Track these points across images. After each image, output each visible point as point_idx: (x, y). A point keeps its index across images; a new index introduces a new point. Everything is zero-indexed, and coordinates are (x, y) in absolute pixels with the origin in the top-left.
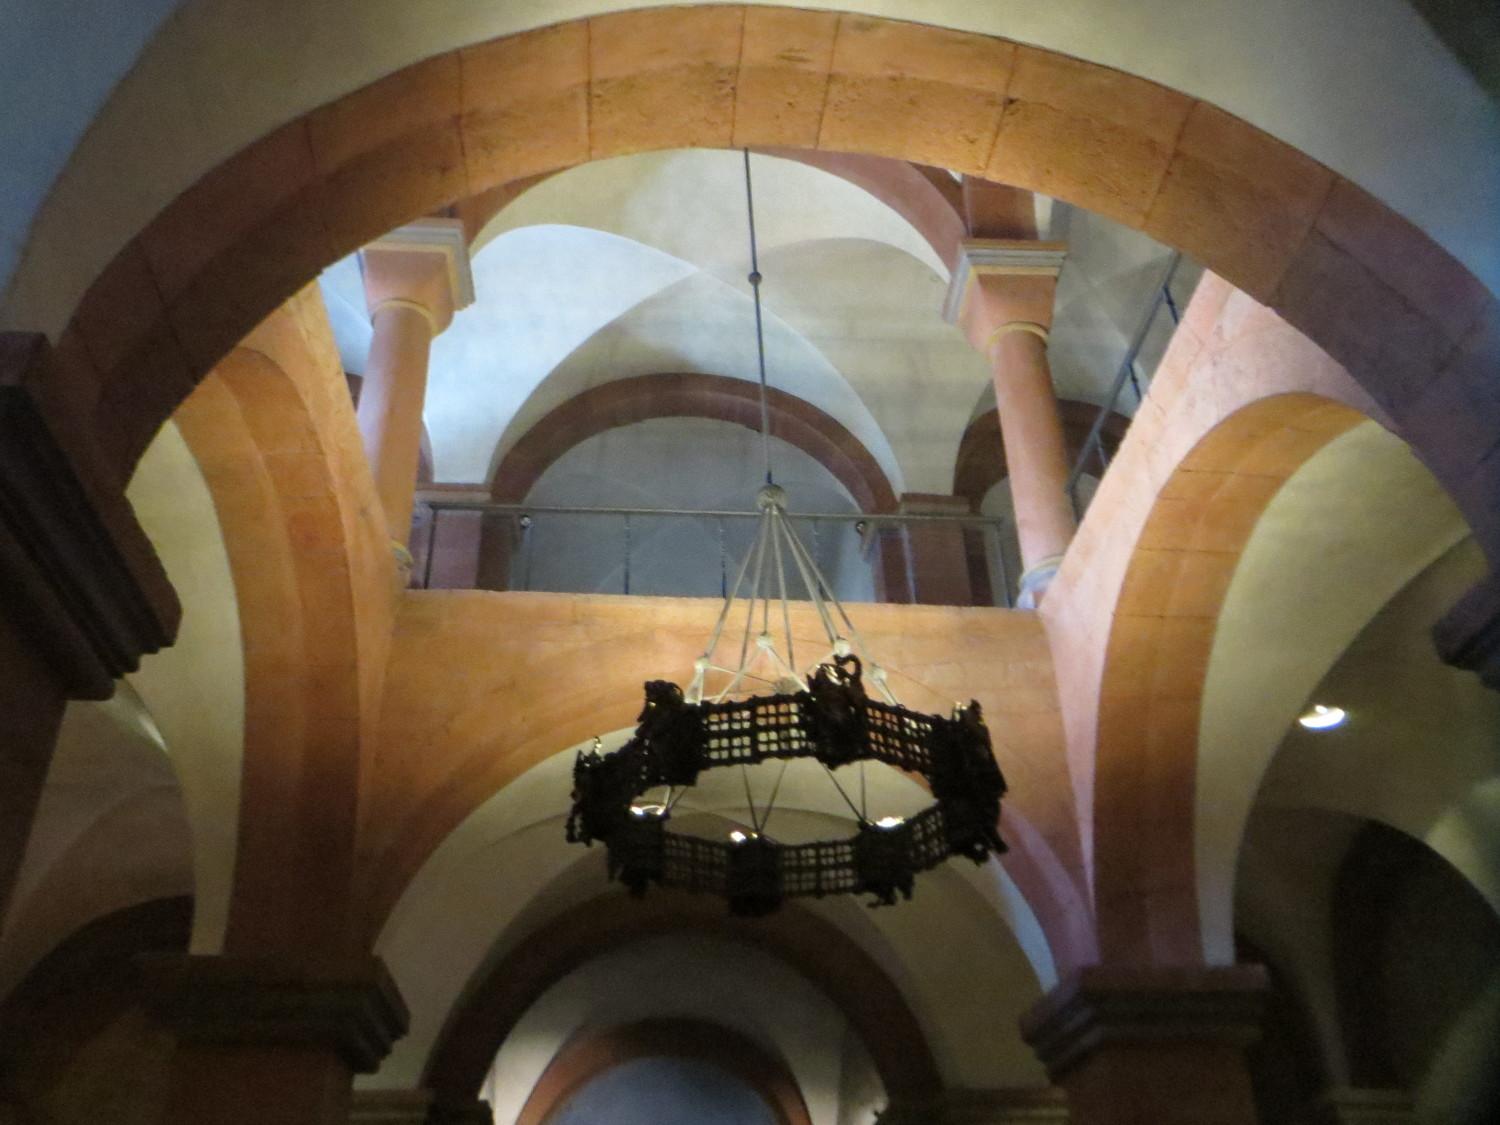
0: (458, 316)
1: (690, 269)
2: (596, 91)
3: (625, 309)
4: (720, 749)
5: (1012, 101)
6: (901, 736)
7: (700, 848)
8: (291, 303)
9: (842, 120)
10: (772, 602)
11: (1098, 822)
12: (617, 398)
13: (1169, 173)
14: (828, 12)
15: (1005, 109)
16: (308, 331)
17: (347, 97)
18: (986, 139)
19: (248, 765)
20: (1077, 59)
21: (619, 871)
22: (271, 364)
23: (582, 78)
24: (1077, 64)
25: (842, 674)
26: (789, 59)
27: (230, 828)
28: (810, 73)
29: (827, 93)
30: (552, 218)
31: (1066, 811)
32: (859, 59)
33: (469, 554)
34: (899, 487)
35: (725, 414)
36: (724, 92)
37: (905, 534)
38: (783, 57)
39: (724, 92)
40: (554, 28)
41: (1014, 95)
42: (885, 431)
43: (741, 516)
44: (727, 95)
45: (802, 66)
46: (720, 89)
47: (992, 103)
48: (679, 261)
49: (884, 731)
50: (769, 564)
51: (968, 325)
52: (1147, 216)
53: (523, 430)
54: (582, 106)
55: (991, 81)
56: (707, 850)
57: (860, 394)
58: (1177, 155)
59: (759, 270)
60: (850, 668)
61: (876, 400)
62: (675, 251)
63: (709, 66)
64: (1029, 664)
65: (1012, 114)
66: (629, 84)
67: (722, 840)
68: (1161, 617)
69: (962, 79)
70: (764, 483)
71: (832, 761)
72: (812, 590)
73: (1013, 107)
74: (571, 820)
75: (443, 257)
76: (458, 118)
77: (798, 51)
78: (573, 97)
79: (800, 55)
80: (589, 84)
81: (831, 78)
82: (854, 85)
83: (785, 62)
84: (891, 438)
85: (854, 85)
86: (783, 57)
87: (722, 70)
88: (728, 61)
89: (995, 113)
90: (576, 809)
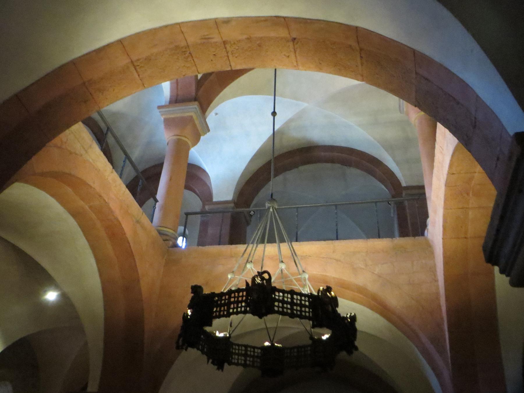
0: (202, 137)
1: (305, 105)
2: (136, 64)
3: (281, 124)
4: (278, 307)
5: (295, 39)
6: (292, 304)
7: (249, 349)
8: (34, 159)
9: (236, 57)
10: (281, 245)
11: (450, 332)
12: (287, 160)
13: (361, 57)
14: (210, 19)
15: (293, 42)
16: (92, 160)
17: (33, 84)
18: (292, 55)
19: (106, 319)
20: (309, 19)
21: (211, 361)
22: (70, 174)
23: (128, 61)
24: (308, 21)
25: (263, 279)
26: (205, 39)
27: (101, 345)
28: (216, 42)
29: (226, 48)
30: (242, 94)
31: (439, 325)
32: (230, 33)
33: (226, 229)
34: (404, 184)
35: (332, 161)
36: (187, 55)
37: (406, 203)
38: (202, 39)
39: (187, 55)
40: (108, 46)
41: (294, 36)
42: (394, 161)
43: (289, 208)
44: (188, 56)
45: (210, 40)
46: (185, 54)
47: (288, 41)
48: (300, 102)
49: (283, 302)
50: (271, 230)
51: (408, 114)
52: (362, 76)
53: (248, 178)
54: (132, 69)
55: (283, 33)
56: (252, 350)
57: (383, 147)
58: (361, 50)
59: (276, 111)
60: (266, 276)
61: (389, 148)
62: (296, 98)
63: (177, 47)
64: (424, 261)
65: (297, 44)
66: (148, 59)
67: (259, 345)
68: (466, 238)
69: (273, 34)
70: (270, 197)
71: (261, 316)
72: (277, 241)
73: (296, 41)
74: (179, 340)
75: (192, 117)
76: (84, 83)
77: (207, 35)
78: (128, 68)
79: (209, 36)
80: (132, 62)
81: (225, 43)
82: (234, 43)
83: (204, 41)
84: (398, 164)
85: (234, 43)
86: (202, 39)
87: (182, 47)
88: (183, 44)
89: (291, 44)
90: (180, 336)
